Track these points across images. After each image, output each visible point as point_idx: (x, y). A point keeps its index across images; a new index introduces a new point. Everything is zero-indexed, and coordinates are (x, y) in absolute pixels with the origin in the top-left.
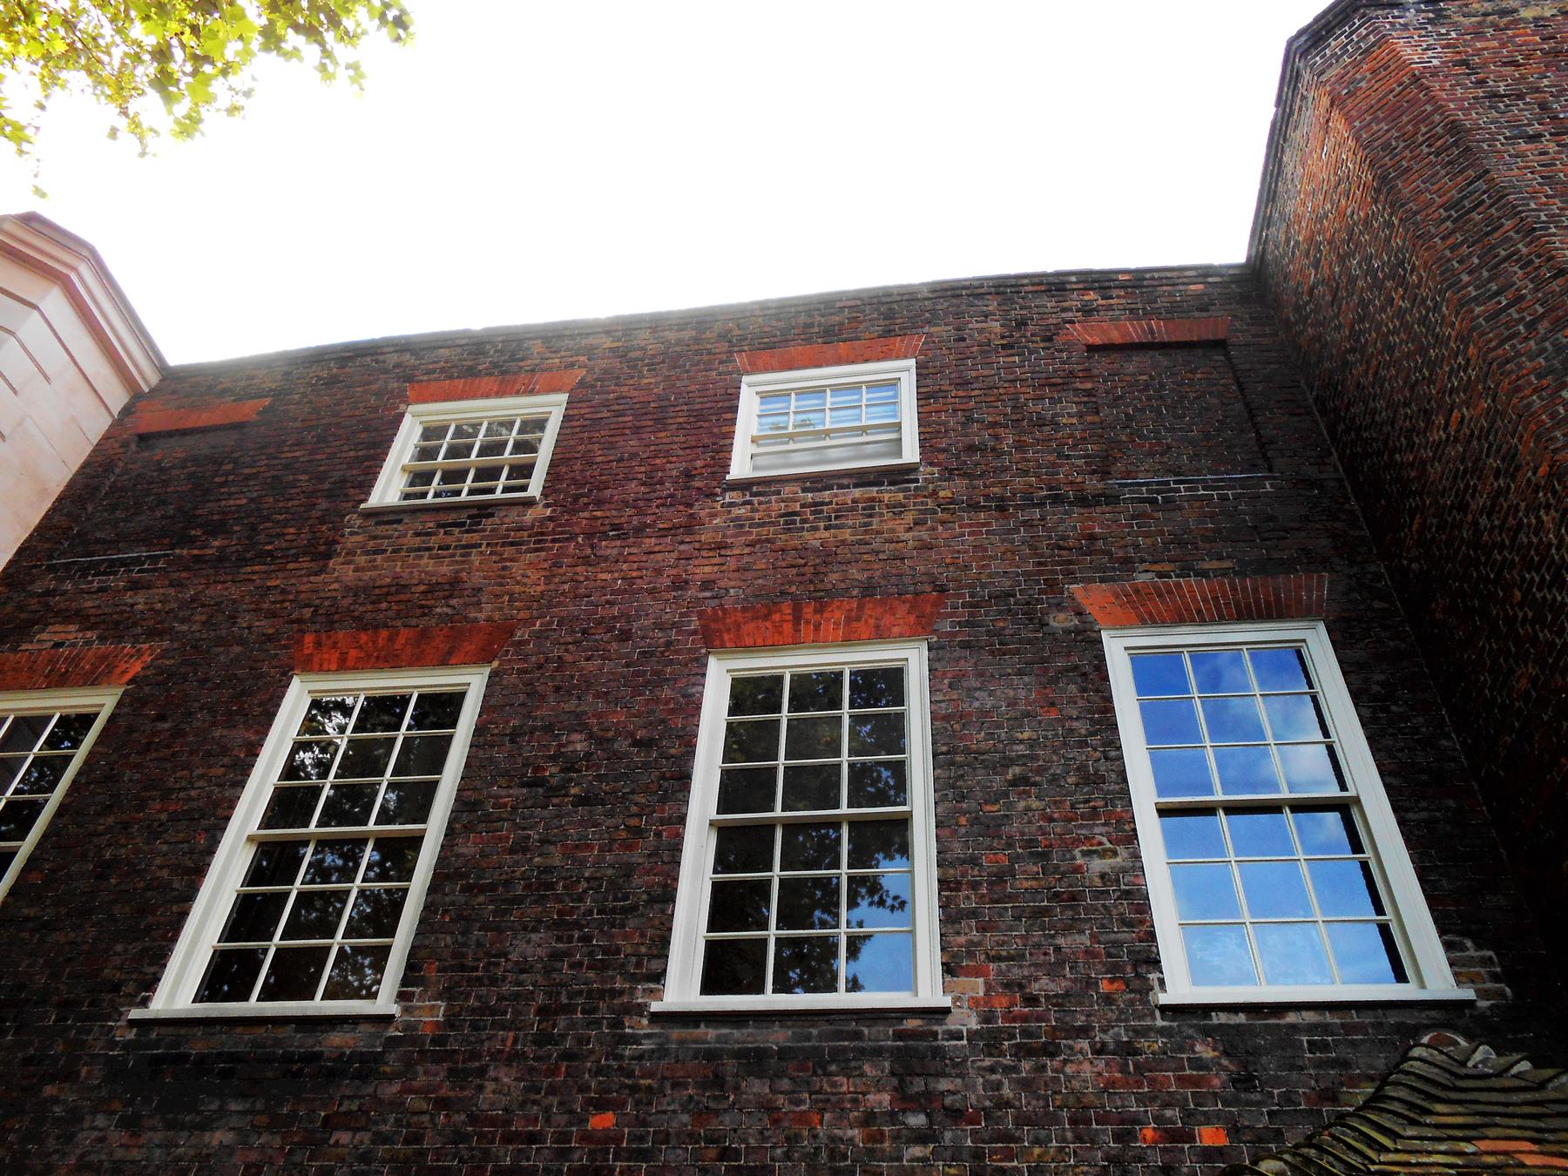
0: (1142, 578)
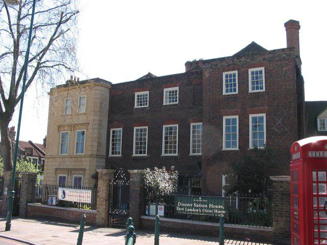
0: (194, 117)
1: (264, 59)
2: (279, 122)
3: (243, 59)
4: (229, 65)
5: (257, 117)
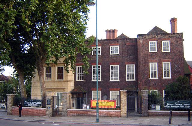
1: (169, 37)
2: (177, 66)
3: (159, 36)
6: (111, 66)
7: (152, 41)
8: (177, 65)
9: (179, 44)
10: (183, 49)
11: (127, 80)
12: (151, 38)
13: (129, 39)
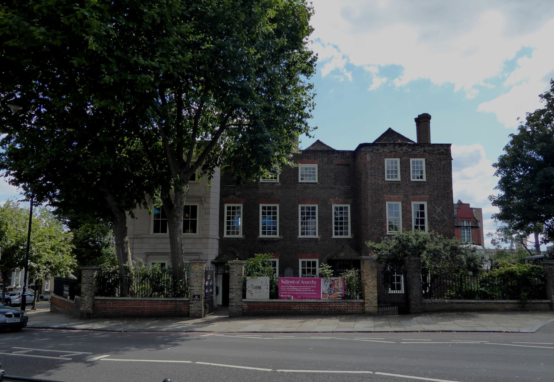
1: (424, 151)
2: (439, 210)
3: (405, 148)
4: (391, 152)
5: (189, 206)
6: (300, 206)
7: (391, 157)
8: (439, 207)
9: (444, 166)
10: (451, 178)
11: (334, 236)
12: (389, 151)
13: (334, 151)
